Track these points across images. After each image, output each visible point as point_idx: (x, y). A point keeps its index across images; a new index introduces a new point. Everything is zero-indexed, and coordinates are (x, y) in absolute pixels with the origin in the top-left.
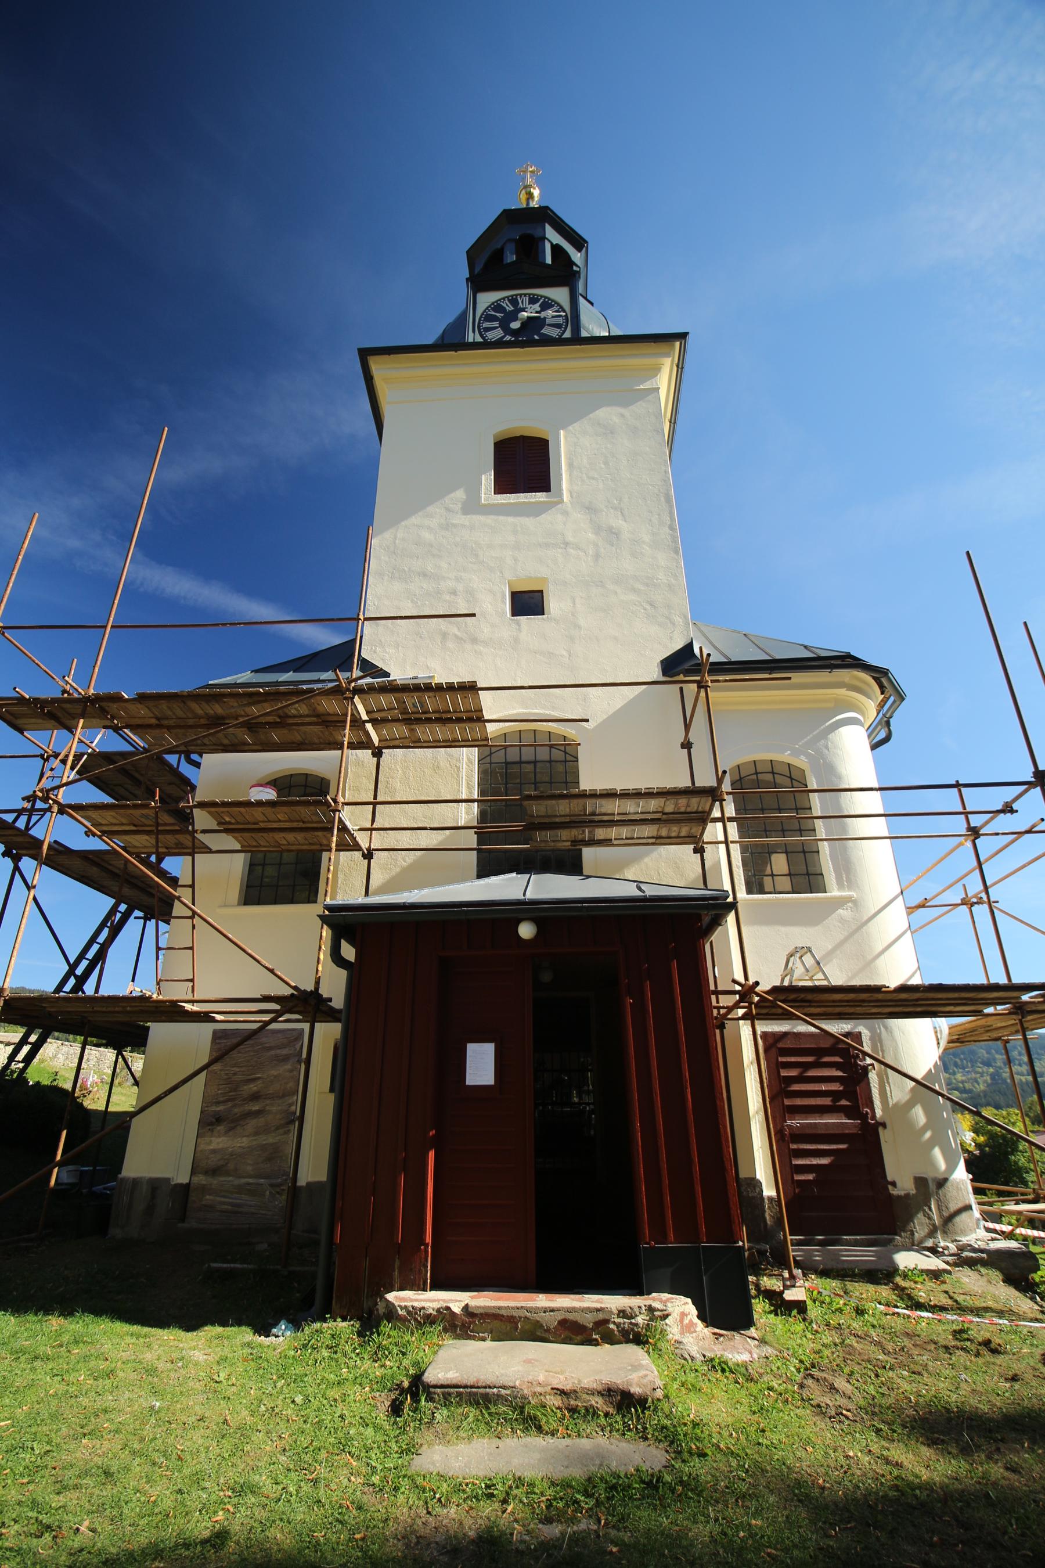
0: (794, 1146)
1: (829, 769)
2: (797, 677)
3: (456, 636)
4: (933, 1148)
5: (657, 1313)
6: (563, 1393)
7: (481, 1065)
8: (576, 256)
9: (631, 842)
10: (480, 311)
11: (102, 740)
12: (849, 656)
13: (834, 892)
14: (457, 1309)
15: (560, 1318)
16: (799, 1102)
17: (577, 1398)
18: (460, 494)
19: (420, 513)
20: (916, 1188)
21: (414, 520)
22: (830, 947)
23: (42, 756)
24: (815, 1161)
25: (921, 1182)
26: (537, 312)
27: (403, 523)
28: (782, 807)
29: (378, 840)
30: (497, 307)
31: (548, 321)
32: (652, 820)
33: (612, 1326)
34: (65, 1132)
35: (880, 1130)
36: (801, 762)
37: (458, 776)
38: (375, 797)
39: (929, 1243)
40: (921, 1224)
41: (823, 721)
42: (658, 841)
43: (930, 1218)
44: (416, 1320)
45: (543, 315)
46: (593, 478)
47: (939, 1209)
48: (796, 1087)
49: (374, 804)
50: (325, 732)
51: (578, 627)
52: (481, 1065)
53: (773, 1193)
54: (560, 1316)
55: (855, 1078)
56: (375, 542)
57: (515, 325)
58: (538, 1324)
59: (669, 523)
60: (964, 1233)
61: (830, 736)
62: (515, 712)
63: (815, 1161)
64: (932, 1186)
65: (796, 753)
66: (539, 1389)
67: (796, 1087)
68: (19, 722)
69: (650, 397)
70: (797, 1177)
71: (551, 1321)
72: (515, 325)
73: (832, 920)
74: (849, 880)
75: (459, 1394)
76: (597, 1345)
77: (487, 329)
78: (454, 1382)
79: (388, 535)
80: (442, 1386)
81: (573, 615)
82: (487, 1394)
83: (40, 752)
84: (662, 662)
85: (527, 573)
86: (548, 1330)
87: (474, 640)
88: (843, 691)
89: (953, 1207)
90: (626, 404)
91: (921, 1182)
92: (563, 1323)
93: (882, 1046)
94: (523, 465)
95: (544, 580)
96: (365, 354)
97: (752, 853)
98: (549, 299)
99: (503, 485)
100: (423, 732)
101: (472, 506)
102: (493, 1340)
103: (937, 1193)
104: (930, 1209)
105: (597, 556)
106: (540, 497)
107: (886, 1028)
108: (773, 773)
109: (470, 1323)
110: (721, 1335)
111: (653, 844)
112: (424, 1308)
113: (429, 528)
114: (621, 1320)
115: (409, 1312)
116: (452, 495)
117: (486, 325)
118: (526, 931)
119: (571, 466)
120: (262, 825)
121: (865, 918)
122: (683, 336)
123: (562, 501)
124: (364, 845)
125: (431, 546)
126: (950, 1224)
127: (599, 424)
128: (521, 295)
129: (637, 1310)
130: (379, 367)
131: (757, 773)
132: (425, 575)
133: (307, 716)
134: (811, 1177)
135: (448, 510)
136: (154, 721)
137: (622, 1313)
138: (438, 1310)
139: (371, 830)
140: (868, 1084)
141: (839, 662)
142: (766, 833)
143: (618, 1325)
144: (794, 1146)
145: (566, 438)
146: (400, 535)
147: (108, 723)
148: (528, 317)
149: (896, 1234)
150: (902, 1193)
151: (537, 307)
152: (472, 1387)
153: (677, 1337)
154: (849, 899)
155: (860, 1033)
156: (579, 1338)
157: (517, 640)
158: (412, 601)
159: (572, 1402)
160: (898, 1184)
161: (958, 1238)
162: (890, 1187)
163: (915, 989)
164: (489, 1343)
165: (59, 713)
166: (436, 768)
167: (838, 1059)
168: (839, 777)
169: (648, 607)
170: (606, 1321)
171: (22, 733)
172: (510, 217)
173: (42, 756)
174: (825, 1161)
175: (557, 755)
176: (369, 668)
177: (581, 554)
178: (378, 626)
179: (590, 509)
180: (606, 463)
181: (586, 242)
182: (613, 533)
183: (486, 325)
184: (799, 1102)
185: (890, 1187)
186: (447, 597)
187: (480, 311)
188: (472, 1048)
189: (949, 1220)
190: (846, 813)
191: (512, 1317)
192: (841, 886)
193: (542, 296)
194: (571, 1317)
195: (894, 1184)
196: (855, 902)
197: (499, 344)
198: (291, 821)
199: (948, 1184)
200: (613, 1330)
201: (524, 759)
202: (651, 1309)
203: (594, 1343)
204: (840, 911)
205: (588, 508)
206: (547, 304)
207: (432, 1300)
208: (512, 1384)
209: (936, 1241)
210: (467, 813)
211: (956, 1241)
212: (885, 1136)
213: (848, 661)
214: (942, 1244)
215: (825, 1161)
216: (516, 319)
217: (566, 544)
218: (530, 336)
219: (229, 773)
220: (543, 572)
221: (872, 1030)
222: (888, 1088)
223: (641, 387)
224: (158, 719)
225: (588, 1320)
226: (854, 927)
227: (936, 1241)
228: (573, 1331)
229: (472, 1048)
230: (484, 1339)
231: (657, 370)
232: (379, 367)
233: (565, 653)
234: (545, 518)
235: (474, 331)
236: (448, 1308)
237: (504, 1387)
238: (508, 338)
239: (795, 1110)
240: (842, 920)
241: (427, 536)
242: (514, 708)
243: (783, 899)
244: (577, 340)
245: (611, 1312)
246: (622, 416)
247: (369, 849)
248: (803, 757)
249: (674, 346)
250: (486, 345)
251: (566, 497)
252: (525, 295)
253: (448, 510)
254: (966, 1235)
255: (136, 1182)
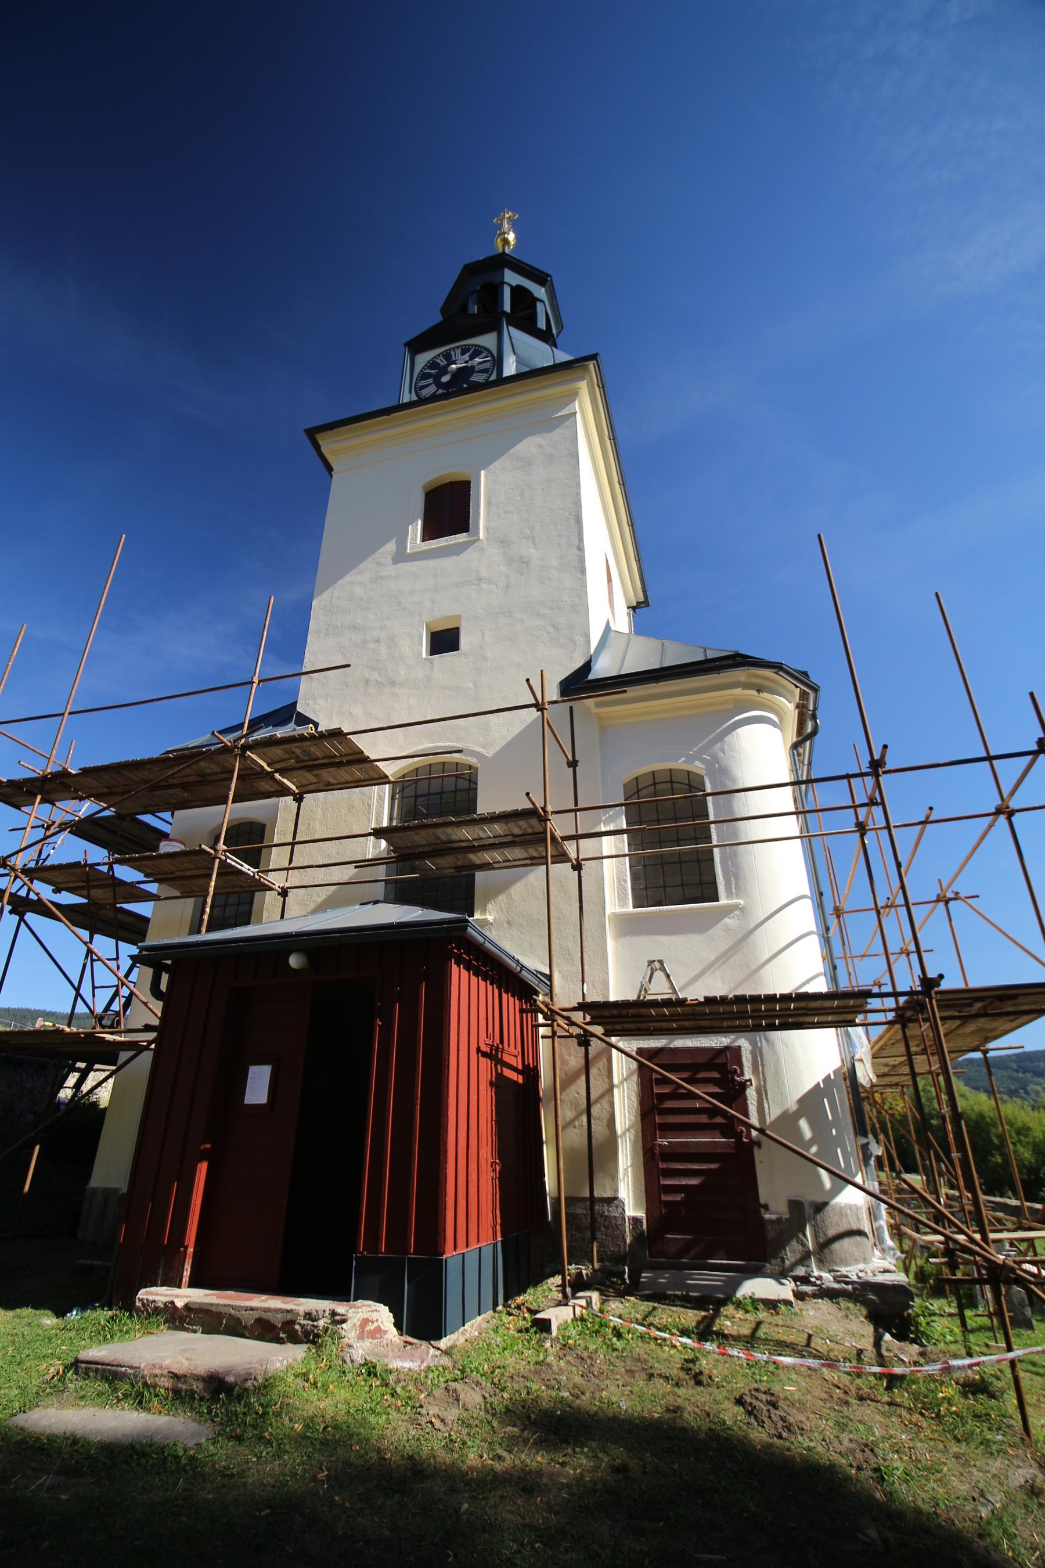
0: (662, 1165)
1: (722, 771)
2: (633, 691)
3: (377, 681)
4: (201, 1160)
5: (337, 1318)
6: (175, 1376)
7: (258, 1084)
8: (539, 292)
9: (508, 864)
10: (417, 370)
11: (86, 808)
12: (738, 655)
13: (723, 901)
14: (180, 1304)
15: (257, 1317)
16: (672, 1119)
17: (185, 1382)
18: (391, 547)
19: (354, 571)
20: (790, 1212)
21: (349, 578)
22: (713, 958)
23: (43, 826)
24: (684, 1182)
25: (796, 1206)
26: (466, 362)
27: (339, 582)
28: (661, 817)
29: (295, 878)
30: (432, 364)
31: (477, 368)
32: (500, 843)
33: (297, 1327)
34: (38, 1147)
35: (756, 1150)
36: (698, 767)
37: (369, 813)
38: (294, 838)
39: (800, 1271)
40: (793, 1251)
41: (721, 723)
42: (534, 862)
43: (803, 1245)
44: (147, 1311)
45: (470, 364)
46: (509, 512)
47: (816, 1235)
48: (669, 1104)
49: (293, 844)
50: (254, 786)
51: (485, 658)
52: (258, 1084)
53: (641, 1214)
54: (256, 1315)
55: (734, 1092)
56: (314, 603)
57: (445, 379)
58: (238, 1321)
59: (576, 544)
60: (845, 1262)
61: (727, 739)
62: (422, 747)
63: (684, 1182)
64: (808, 1210)
65: (690, 760)
66: (158, 1372)
67: (669, 1104)
68: (14, 800)
69: (568, 423)
70: (664, 1198)
71: (248, 1318)
72: (445, 379)
73: (717, 930)
74: (737, 887)
75: (97, 1370)
76: (283, 1343)
77: (423, 388)
78: (97, 1359)
79: (326, 595)
80: (87, 1362)
81: (481, 648)
82: (116, 1372)
83: (40, 823)
84: (561, 683)
85: (441, 614)
86: (246, 1327)
87: (392, 683)
88: (738, 691)
89: (831, 1232)
90: (550, 430)
91: (796, 1206)
92: (259, 1321)
93: (762, 1061)
94: (448, 510)
95: (459, 617)
96: (312, 433)
97: (645, 866)
98: (479, 346)
99: (431, 532)
100: (327, 775)
101: (401, 556)
102: (203, 1333)
103: (815, 1219)
104: (805, 1236)
105: (508, 587)
106: (461, 538)
107: (767, 1040)
108: (671, 782)
109: (187, 1316)
110: (411, 1344)
111: (532, 865)
112: (154, 1301)
113: (361, 583)
114: (306, 1322)
115: (143, 1304)
116: (383, 549)
117: (422, 383)
118: (294, 961)
119: (489, 503)
120: (179, 874)
121: (752, 926)
122: (594, 357)
123: (479, 539)
124: (573, 855)
125: (362, 600)
126: (826, 1251)
127: (518, 458)
128: (454, 349)
129: (321, 1314)
130: (329, 444)
131: (655, 784)
132: (355, 628)
133: (222, 773)
134: (678, 1197)
135: (378, 564)
136: (105, 790)
137: (308, 1316)
138: (165, 1304)
139: (287, 869)
140: (745, 1099)
141: (731, 662)
142: (661, 843)
143: (302, 1326)
144: (662, 1165)
145: (486, 476)
146: (336, 594)
147: (74, 795)
148: (458, 369)
149: (766, 1261)
150: (774, 1217)
151: (466, 357)
152: (108, 1365)
153: (351, 1342)
154: (736, 907)
155: (740, 1047)
156: (269, 1336)
157: (429, 679)
158: (342, 654)
159: (180, 1385)
160: (772, 1206)
161: (836, 1268)
162: (762, 1211)
163: (724, 1000)
164: (199, 1335)
165: (52, 786)
166: (351, 807)
167: (716, 1075)
168: (734, 781)
169: (551, 630)
170: (293, 1322)
171: (19, 809)
172: (472, 270)
173: (43, 826)
174: (694, 1182)
175: (463, 784)
176: (303, 720)
177: (493, 587)
178: (311, 678)
179: (504, 543)
180: (522, 495)
181: (549, 276)
182: (525, 562)
183: (422, 383)
184: (672, 1119)
185: (762, 1211)
186: (372, 646)
187: (417, 370)
188: (253, 1069)
189: (825, 1245)
190: (739, 816)
191: (220, 1313)
192: (729, 895)
193: (472, 345)
194: (265, 1316)
195: (766, 1207)
196: (742, 909)
197: (433, 398)
198: (199, 869)
199: (828, 1208)
200: (297, 1331)
201: (432, 791)
202: (334, 1313)
203: (279, 1341)
204: (727, 920)
205: (502, 542)
206: (477, 351)
207: (184, 1296)
208: (137, 1365)
209: (809, 1269)
210: (374, 847)
211: (834, 1271)
212: (760, 1155)
213: (737, 660)
214: (816, 1273)
215: (694, 1182)
216: (446, 373)
217: (480, 579)
218: (461, 385)
219: (181, 826)
220: (456, 609)
221: (754, 1044)
222: (766, 1105)
223: (560, 414)
224: (107, 787)
225: (278, 1320)
226: (740, 936)
227: (809, 1269)
228: (266, 1330)
229: (253, 1069)
230: (195, 1331)
231: (574, 395)
232: (329, 444)
233: (471, 685)
234: (464, 556)
235: (410, 392)
236: (172, 1302)
237: (131, 1367)
238: (440, 391)
239: (667, 1129)
240: (728, 929)
241: (359, 591)
242: (422, 743)
243: (666, 911)
244: (502, 381)
245: (298, 1314)
246: (540, 446)
247: (577, 860)
248: (697, 763)
249: (587, 368)
250: (421, 402)
251: (482, 535)
252: (458, 347)
253: (378, 564)
254: (847, 1265)
255: (94, 1190)
